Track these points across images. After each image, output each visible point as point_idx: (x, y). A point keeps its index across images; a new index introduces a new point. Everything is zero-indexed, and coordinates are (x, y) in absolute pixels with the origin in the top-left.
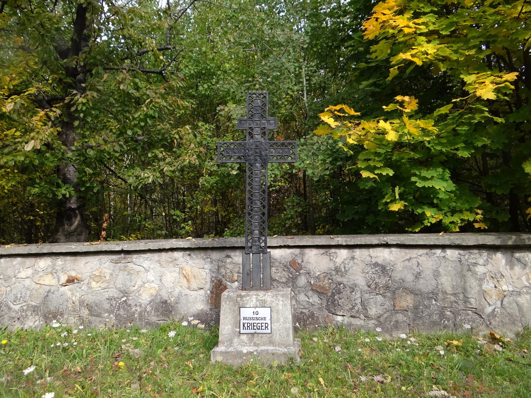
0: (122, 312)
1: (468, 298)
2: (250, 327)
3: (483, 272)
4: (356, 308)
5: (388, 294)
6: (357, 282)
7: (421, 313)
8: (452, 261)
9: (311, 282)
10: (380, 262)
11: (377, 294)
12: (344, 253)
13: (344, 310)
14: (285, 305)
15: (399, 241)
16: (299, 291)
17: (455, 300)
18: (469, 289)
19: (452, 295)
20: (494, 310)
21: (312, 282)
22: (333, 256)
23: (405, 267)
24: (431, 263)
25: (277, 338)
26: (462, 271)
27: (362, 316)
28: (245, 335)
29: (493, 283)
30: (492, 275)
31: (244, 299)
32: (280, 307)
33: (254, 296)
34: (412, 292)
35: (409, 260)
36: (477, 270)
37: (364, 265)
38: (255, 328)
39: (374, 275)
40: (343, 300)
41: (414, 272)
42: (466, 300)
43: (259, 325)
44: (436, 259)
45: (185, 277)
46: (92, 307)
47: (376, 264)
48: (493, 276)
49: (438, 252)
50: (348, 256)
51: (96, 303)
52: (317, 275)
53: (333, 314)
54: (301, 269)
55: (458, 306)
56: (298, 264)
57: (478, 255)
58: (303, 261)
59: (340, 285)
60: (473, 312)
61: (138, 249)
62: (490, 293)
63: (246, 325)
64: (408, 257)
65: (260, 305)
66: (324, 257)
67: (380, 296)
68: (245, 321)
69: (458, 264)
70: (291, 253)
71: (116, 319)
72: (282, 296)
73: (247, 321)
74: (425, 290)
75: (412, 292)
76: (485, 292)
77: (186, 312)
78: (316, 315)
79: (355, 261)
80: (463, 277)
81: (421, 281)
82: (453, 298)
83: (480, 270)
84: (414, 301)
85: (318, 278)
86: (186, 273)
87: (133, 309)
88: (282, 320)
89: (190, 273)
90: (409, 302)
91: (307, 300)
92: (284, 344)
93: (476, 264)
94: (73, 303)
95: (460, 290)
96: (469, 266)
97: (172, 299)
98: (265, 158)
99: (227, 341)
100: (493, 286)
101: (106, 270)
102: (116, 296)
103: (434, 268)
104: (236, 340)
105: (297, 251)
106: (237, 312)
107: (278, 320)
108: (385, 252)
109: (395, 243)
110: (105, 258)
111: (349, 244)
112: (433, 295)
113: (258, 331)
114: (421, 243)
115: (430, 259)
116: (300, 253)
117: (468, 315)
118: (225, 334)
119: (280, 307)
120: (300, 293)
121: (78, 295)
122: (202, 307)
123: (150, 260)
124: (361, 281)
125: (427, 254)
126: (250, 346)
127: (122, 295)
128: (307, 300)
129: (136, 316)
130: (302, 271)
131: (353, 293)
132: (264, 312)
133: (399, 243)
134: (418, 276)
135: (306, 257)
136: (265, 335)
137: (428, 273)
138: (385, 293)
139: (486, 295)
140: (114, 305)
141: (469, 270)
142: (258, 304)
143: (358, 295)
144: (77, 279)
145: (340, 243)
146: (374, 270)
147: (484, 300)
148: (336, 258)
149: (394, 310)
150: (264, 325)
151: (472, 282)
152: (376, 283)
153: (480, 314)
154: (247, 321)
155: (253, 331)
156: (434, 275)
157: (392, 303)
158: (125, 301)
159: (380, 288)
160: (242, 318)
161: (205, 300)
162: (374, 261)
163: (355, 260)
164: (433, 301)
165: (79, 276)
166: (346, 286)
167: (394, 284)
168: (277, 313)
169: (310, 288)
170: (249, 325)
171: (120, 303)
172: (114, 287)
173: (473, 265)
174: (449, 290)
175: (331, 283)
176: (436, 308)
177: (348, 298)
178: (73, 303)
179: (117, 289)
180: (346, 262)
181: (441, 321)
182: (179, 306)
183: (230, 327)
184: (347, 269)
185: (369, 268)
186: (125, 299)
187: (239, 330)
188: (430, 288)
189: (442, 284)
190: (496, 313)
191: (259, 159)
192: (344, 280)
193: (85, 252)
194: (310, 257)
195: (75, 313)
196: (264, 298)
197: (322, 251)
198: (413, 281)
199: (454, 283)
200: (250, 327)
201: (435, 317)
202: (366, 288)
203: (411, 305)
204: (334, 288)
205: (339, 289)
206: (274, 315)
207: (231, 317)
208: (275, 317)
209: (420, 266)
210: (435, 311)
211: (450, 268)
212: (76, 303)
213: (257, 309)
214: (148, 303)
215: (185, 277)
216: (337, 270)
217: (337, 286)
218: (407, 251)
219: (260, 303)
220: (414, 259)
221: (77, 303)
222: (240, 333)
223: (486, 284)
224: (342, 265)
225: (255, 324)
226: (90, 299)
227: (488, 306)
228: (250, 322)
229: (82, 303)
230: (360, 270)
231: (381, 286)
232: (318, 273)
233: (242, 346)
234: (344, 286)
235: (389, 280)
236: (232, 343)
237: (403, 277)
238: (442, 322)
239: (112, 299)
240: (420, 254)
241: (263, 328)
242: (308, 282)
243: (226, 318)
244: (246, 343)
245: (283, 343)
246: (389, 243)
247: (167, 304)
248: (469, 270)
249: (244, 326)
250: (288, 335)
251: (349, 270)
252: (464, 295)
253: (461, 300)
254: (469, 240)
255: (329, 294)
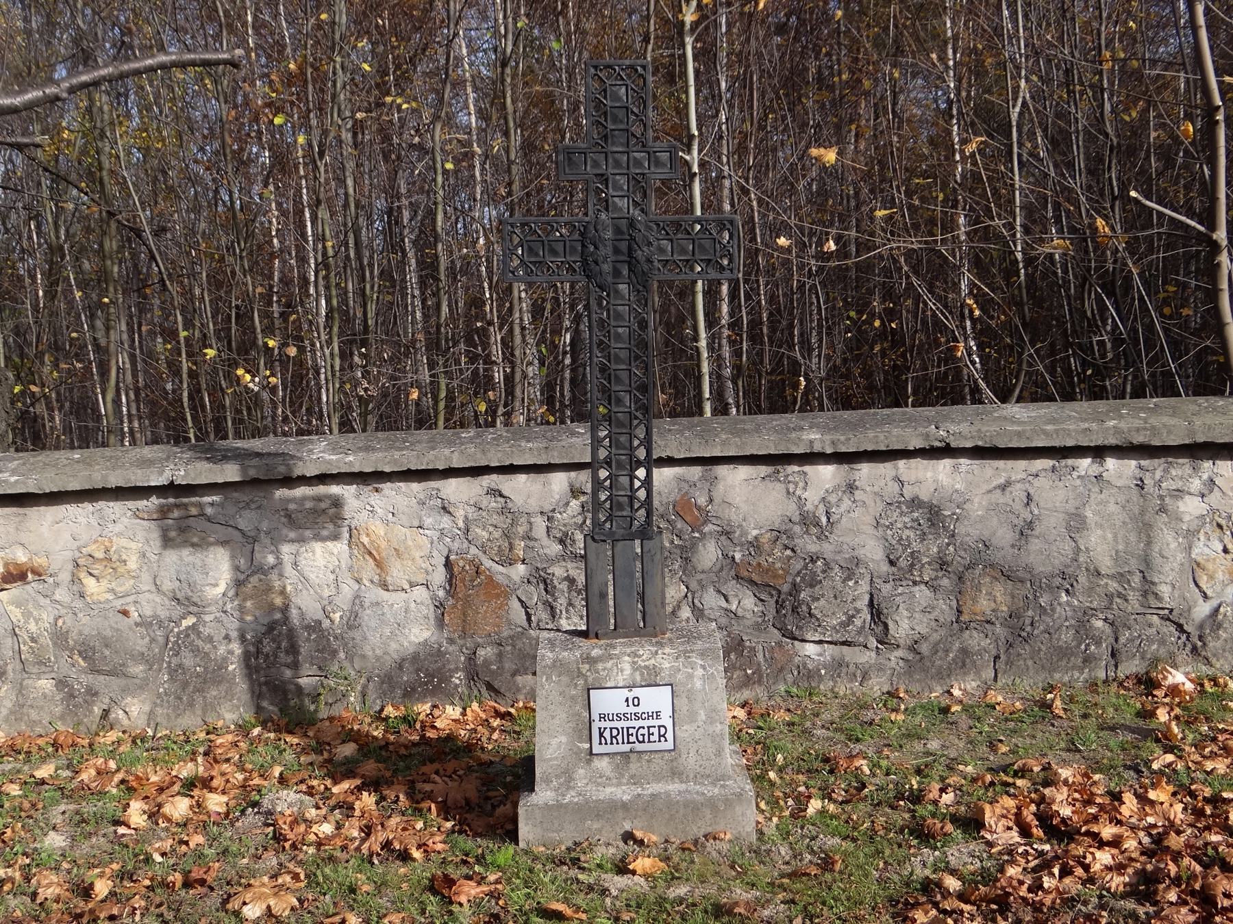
0: (188, 660)
1: (1153, 583)
2: (620, 738)
3: (1198, 512)
4: (858, 622)
5: (945, 582)
6: (860, 553)
7: (1028, 629)
8: (1119, 488)
9: (733, 558)
10: (924, 497)
11: (915, 583)
12: (826, 474)
13: (824, 628)
14: (708, 678)
15: (980, 438)
16: (700, 582)
17: (1121, 589)
18: (1158, 560)
19: (1112, 577)
20: (1217, 610)
21: (738, 556)
22: (796, 484)
23: (993, 508)
24: (1062, 494)
25: (692, 761)
26: (1143, 512)
27: (873, 643)
28: (606, 759)
29: (1221, 541)
30: (1220, 520)
31: (600, 666)
32: (698, 684)
33: (627, 658)
34: (1007, 575)
35: (1003, 488)
36: (1182, 509)
37: (881, 506)
38: (632, 739)
39: (907, 532)
40: (822, 602)
41: (1016, 521)
42: (1148, 590)
43: (641, 731)
44: (1078, 482)
45: (370, 554)
46: (93, 649)
47: (915, 503)
48: (1223, 523)
49: (1085, 463)
50: (837, 481)
51: (105, 638)
52: (750, 538)
53: (795, 639)
54: (705, 522)
55: (1123, 605)
56: (699, 508)
57: (1188, 470)
58: (711, 501)
59: (813, 561)
60: (1162, 618)
61: (220, 481)
62: (1210, 566)
63: (607, 734)
64: (1002, 481)
65: (643, 679)
66: (771, 485)
67: (923, 587)
68: (603, 724)
69: (1135, 491)
70: (680, 480)
71: (172, 679)
72: (703, 654)
73: (609, 724)
74: (1042, 568)
75: (1007, 575)
76: (1198, 565)
77: (378, 652)
78: (748, 644)
79: (858, 495)
80: (1146, 530)
81: (1035, 544)
82: (1113, 586)
83: (1191, 507)
84: (1013, 597)
85: (755, 544)
86: (372, 542)
87: (222, 650)
88: (702, 716)
89: (383, 544)
90: (999, 599)
91: (724, 604)
92: (709, 776)
93: (1179, 493)
94: (33, 640)
95: (1134, 564)
96: (1161, 498)
97: (337, 617)
98: (646, 268)
99: (557, 777)
100: (1220, 548)
101: (124, 542)
102: (163, 614)
103: (1070, 507)
104: (581, 771)
105: (696, 472)
106: (581, 701)
107: (692, 717)
108: (941, 467)
109: (969, 445)
110: (114, 509)
111: (843, 449)
112: (1066, 580)
113: (639, 747)
114: (1040, 444)
115: (1061, 484)
116: (703, 478)
117: (1150, 626)
118: (551, 759)
119: (698, 684)
120: (703, 587)
121: (45, 616)
122: (426, 634)
123: (259, 508)
124: (873, 552)
125: (1054, 469)
126: (619, 785)
127: (180, 610)
128: (724, 604)
129: (231, 668)
130: (707, 528)
131: (851, 583)
132: (657, 700)
133: (980, 443)
134: (1025, 531)
135: (721, 487)
136: (660, 755)
137: (1052, 524)
138: (936, 578)
139: (1199, 572)
140: (161, 640)
141: (1163, 509)
142: (638, 678)
143: (864, 587)
144: (34, 572)
145: (817, 448)
146: (907, 520)
147: (1192, 585)
148: (805, 489)
149: (960, 622)
150: (655, 731)
151: (1168, 541)
152: (912, 553)
153: (1182, 621)
154: (609, 724)
155: (627, 748)
156: (1069, 528)
157: (954, 603)
158: (193, 627)
159: (923, 565)
160: (595, 716)
161: (432, 616)
162: (908, 492)
163: (857, 493)
164: (1063, 595)
165: (40, 561)
166: (832, 565)
167: (962, 553)
168: (688, 698)
169: (733, 573)
170: (615, 732)
171: (179, 633)
172: (153, 588)
173: (1171, 496)
174: (1106, 564)
175: (789, 558)
176: (1070, 614)
177: (835, 597)
178: (33, 640)
179: (165, 594)
180: (833, 499)
181: (1080, 644)
182: (356, 634)
183: (564, 739)
184: (834, 518)
185: (896, 514)
186: (189, 621)
187: (587, 746)
188: (1057, 563)
189: (1087, 549)
190: (1220, 617)
191: (625, 272)
192: (827, 549)
193: (52, 493)
194: (733, 487)
195: (43, 668)
196: (652, 661)
197: (764, 470)
198: (1013, 546)
199: (1121, 547)
200: (620, 738)
201: (1067, 637)
202: (885, 568)
203: (1005, 609)
204: (799, 573)
205: (814, 574)
206: (682, 703)
207: (564, 716)
208: (685, 709)
209: (1033, 505)
210: (1066, 619)
211: (1112, 507)
212: (42, 640)
213: (637, 692)
214: (263, 629)
215: (370, 554)
216: (808, 521)
217: (806, 567)
218: (1000, 463)
219: (642, 674)
220: (1019, 486)
221: (46, 640)
222: (591, 753)
223: (1201, 544)
224: (822, 509)
225: (631, 731)
226: (84, 625)
227: (1201, 600)
228: (619, 725)
229: (60, 637)
230: (869, 519)
231: (925, 560)
232: (755, 532)
233: (599, 784)
234: (827, 564)
235: (948, 545)
236: (570, 779)
237: (986, 534)
238: (1083, 647)
239: (151, 623)
240: (1034, 471)
241: (655, 737)
242: (725, 556)
243: (553, 717)
244: (609, 779)
245: (708, 772)
246: (953, 445)
247: (322, 630)
248: (1163, 509)
249: (601, 735)
250: (719, 753)
251: (839, 521)
252: (1144, 577)
253: (1133, 589)
254: (1169, 432)
255: (786, 588)
